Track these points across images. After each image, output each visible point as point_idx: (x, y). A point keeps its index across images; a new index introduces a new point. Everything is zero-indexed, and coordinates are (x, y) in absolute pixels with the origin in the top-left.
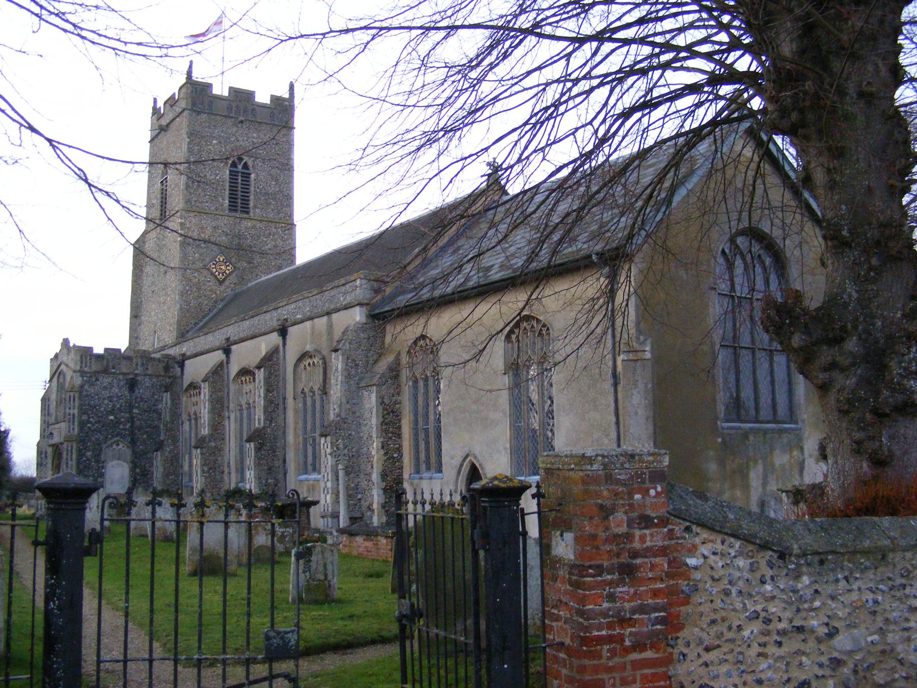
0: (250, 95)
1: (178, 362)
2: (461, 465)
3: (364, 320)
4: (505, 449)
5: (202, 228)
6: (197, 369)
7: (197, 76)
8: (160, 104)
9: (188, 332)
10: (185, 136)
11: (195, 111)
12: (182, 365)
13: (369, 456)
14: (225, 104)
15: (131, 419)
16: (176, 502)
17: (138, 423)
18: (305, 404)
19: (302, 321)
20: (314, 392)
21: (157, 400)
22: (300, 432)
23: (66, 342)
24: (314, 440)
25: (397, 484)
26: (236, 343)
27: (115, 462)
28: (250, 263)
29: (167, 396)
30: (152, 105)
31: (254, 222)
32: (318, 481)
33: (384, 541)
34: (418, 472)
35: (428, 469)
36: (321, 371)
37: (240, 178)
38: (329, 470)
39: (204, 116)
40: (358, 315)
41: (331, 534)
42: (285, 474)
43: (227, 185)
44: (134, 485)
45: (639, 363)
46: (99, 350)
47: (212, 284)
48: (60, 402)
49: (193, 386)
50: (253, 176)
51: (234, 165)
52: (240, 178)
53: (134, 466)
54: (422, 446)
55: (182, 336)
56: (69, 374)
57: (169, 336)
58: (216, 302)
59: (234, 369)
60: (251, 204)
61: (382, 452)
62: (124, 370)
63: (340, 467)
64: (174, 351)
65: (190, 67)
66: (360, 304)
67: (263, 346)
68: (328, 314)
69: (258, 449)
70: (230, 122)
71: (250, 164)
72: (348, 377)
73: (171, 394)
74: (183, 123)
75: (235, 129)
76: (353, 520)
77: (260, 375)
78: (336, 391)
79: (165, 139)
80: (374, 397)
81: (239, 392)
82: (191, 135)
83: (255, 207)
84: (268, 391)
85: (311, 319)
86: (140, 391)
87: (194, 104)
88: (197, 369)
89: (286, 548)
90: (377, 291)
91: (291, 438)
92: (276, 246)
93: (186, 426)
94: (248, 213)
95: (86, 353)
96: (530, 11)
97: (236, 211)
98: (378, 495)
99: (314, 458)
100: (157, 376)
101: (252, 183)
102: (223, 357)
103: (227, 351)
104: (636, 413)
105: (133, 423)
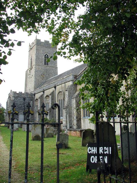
6: (37, 96)
7: (38, 38)
8: (31, 44)
12: (34, 95)
13: (74, 113)
14: (43, 43)
18: (60, 102)
19: (59, 85)
20: (62, 100)
23: (11, 90)
24: (62, 110)
25: (80, 119)
26: (45, 90)
27: (21, 115)
29: (32, 102)
30: (29, 44)
32: (63, 119)
33: (78, 132)
34: (84, 117)
35: (87, 116)
36: (63, 95)
38: (65, 116)
41: (66, 130)
42: (56, 117)
44: (25, 120)
46: (18, 92)
48: (10, 103)
49: (37, 99)
51: (45, 55)
55: (35, 88)
56: (12, 97)
57: (32, 90)
59: (45, 96)
61: (77, 112)
62: (23, 96)
63: (68, 115)
64: (33, 93)
67: (51, 90)
68: (65, 83)
70: (45, 47)
72: (69, 96)
74: (35, 47)
76: (70, 127)
77: (50, 96)
78: (66, 99)
79: (31, 51)
81: (46, 100)
82: (36, 49)
83: (50, 64)
84: (52, 100)
85: (61, 84)
87: (37, 43)
88: (37, 96)
89: (55, 133)
93: (35, 108)
95: (15, 93)
97: (46, 65)
98: (76, 122)
99: (62, 114)
102: (43, 93)
103: (44, 92)
105: (24, 107)
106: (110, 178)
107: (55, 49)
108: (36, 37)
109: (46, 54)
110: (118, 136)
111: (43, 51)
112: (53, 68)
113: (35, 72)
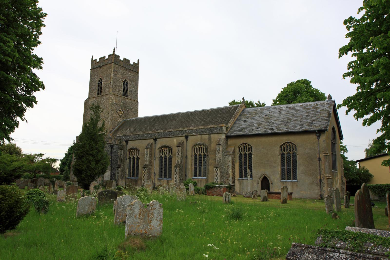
1: (126, 141)
2: (261, 177)
7: (117, 53)
9: (112, 131)
10: (112, 71)
11: (115, 64)
12: (127, 142)
16: (218, 183)
17: (113, 159)
22: (193, 165)
28: (127, 112)
30: (92, 58)
31: (129, 100)
37: (126, 85)
40: (223, 136)
43: (123, 87)
45: (327, 156)
47: (118, 117)
50: (129, 86)
51: (124, 82)
53: (111, 171)
60: (128, 95)
62: (110, 142)
65: (114, 50)
69: (179, 169)
70: (124, 68)
71: (128, 82)
73: (123, 151)
75: (125, 71)
80: (230, 158)
83: (129, 95)
86: (114, 149)
91: (189, 167)
92: (134, 107)
97: (124, 96)
100: (118, 145)
101: (129, 88)
104: (327, 167)
105: (111, 158)
106: (226, 194)
107: (136, 73)
108: (114, 51)
111: (122, 74)
112: (133, 101)
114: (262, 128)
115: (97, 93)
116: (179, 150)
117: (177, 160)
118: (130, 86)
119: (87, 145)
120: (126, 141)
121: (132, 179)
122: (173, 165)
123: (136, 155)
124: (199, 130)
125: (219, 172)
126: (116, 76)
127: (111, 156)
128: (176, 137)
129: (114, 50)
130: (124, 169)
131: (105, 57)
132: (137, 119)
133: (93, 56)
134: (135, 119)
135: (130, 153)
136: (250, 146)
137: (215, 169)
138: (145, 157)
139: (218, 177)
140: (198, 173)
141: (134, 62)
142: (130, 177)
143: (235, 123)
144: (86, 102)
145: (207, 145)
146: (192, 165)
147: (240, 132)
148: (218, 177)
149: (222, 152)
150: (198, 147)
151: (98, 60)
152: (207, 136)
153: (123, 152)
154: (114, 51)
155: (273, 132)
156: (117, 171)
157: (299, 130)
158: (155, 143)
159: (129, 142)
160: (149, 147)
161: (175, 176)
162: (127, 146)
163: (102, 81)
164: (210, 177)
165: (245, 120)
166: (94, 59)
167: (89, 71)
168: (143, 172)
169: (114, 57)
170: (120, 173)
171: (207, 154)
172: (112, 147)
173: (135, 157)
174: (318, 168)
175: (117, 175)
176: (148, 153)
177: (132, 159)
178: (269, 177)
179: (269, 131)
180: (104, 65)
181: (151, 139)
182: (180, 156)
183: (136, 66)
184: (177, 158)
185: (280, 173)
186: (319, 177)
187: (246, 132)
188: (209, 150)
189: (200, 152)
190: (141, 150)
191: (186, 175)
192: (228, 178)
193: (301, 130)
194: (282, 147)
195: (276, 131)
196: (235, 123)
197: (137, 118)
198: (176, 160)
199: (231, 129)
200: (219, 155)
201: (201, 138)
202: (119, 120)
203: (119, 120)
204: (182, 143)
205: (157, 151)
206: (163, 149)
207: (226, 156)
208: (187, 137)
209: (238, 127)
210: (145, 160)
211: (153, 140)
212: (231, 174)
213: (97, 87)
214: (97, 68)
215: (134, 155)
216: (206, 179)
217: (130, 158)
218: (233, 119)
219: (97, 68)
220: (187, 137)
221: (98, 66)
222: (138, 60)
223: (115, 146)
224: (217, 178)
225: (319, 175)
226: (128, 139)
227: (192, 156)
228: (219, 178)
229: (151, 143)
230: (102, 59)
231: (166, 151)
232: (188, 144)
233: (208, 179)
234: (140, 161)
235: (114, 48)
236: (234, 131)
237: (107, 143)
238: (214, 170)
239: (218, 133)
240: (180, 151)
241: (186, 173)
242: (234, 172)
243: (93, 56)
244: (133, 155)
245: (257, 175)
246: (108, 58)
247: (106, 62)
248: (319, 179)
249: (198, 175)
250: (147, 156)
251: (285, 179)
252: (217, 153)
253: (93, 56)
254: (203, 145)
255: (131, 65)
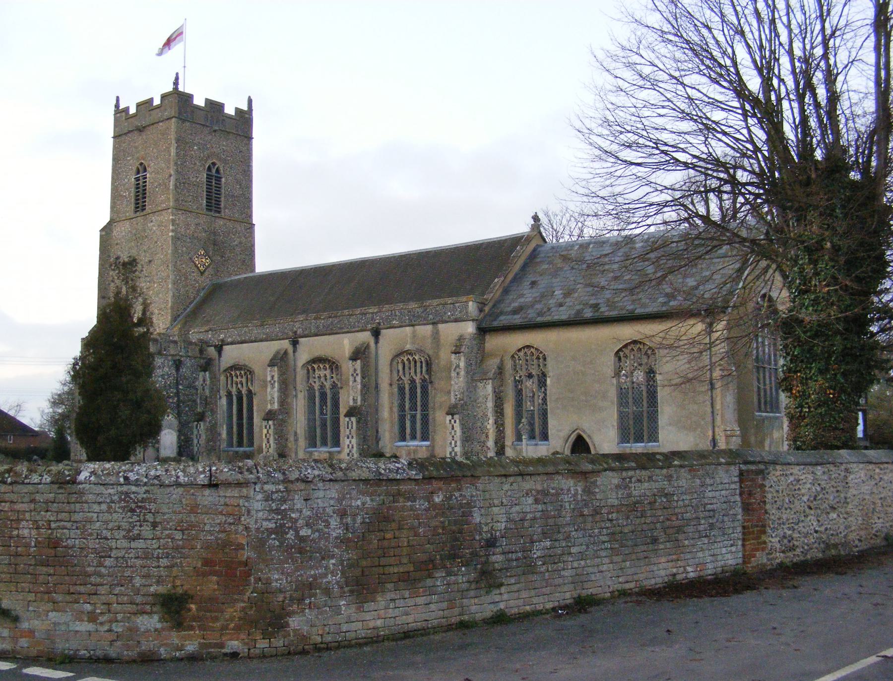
0: (221, 106)
1: (216, 346)
2: (569, 436)
3: (475, 331)
4: (613, 426)
5: (188, 225)
10: (173, 142)
12: (219, 349)
15: (177, 394)
21: (195, 378)
22: (396, 409)
30: (115, 102)
31: (225, 221)
34: (519, 438)
37: (214, 178)
39: (188, 124)
40: (470, 328)
50: (223, 180)
51: (209, 169)
52: (214, 181)
53: (180, 432)
54: (408, 424)
58: (198, 291)
62: (172, 352)
65: (177, 79)
66: (473, 320)
69: (358, 422)
70: (206, 130)
75: (210, 137)
80: (489, 388)
83: (225, 208)
86: (183, 370)
87: (180, 113)
90: (481, 310)
91: (385, 413)
92: (240, 243)
94: (219, 212)
96: (663, 152)
97: (211, 210)
100: (195, 358)
103: (295, 343)
105: (178, 397)
108: (176, 83)
109: (214, 164)
110: (170, 427)
112: (237, 225)
113: (174, 244)
114: (571, 304)
115: (133, 206)
116: (355, 370)
117: (351, 398)
118: (227, 180)
119: (617, 519)
120: (216, 346)
121: (237, 452)
122: (343, 410)
123: (244, 385)
124: (406, 311)
125: (457, 426)
126: (185, 155)
127: (177, 388)
128: (348, 332)
129: (177, 79)
130: (216, 423)
131: (152, 100)
132: (254, 277)
133: (118, 99)
134: (246, 278)
135: (229, 379)
136: (541, 352)
137: (449, 417)
138: (269, 389)
139: (456, 442)
140: (408, 431)
141: (236, 109)
142: (232, 446)
143: (506, 291)
144: (104, 233)
145: (431, 353)
146: (391, 408)
147: (516, 317)
148: (456, 442)
149: (467, 373)
150: (405, 359)
151: (133, 111)
152: (430, 327)
153: (211, 379)
154: (176, 83)
155: (596, 314)
156: (195, 432)
157: (659, 309)
158: (377, 342)
159: (226, 348)
160: (279, 360)
161: (347, 442)
162: (376, 348)
163: (145, 170)
164: (438, 438)
165: (534, 279)
166: (122, 106)
167: (110, 142)
168: (265, 431)
169: (179, 100)
170: (204, 437)
171: (430, 377)
172: (178, 365)
173: (244, 391)
174: (709, 410)
175: (195, 441)
176: (276, 378)
177: (234, 398)
178: (589, 436)
179: (588, 314)
180: (148, 126)
181: (283, 339)
182: (359, 387)
183: (244, 118)
184: (351, 392)
185: (615, 424)
186: (710, 433)
187: (531, 315)
188: (434, 367)
189: (413, 374)
190: (257, 370)
191: (377, 437)
192: (484, 442)
193: (664, 309)
194: (621, 354)
195: (605, 311)
196: (506, 291)
197: (251, 275)
198: (350, 396)
199: (494, 306)
200: (458, 383)
201: (414, 335)
202: (198, 282)
203: (198, 282)
204: (364, 351)
205: (301, 374)
206: (316, 366)
207: (479, 384)
208: (376, 333)
209: (513, 300)
210: (269, 398)
211: (287, 341)
212: (491, 431)
213: (133, 194)
214: (129, 132)
215: (239, 386)
216: (427, 447)
217: (229, 395)
218: (502, 279)
219: (129, 132)
220: (376, 333)
221: (132, 125)
222: (250, 101)
223: (188, 363)
224: (453, 442)
225: (710, 428)
226: (222, 341)
227: (391, 385)
228: (458, 443)
229: (282, 352)
230: (145, 106)
231: (323, 372)
232: (379, 352)
233: (433, 447)
234: (255, 402)
235: (177, 74)
236: (502, 313)
237: (166, 355)
238: (445, 420)
239: (456, 321)
240: (359, 372)
241: (377, 432)
242: (503, 425)
243: (118, 98)
244: (237, 384)
245: (560, 431)
246: (159, 102)
247: (156, 116)
248: (711, 438)
249: (408, 437)
250: (273, 388)
251: (628, 442)
252: (453, 374)
253: (118, 98)
254: (420, 351)
255: (229, 117)
